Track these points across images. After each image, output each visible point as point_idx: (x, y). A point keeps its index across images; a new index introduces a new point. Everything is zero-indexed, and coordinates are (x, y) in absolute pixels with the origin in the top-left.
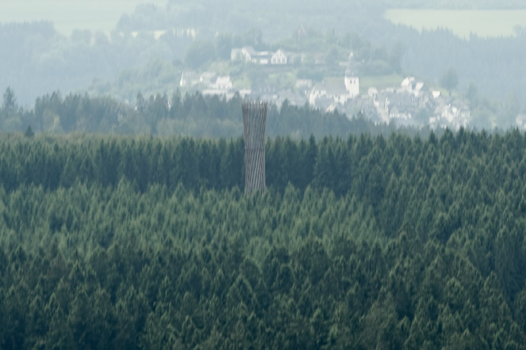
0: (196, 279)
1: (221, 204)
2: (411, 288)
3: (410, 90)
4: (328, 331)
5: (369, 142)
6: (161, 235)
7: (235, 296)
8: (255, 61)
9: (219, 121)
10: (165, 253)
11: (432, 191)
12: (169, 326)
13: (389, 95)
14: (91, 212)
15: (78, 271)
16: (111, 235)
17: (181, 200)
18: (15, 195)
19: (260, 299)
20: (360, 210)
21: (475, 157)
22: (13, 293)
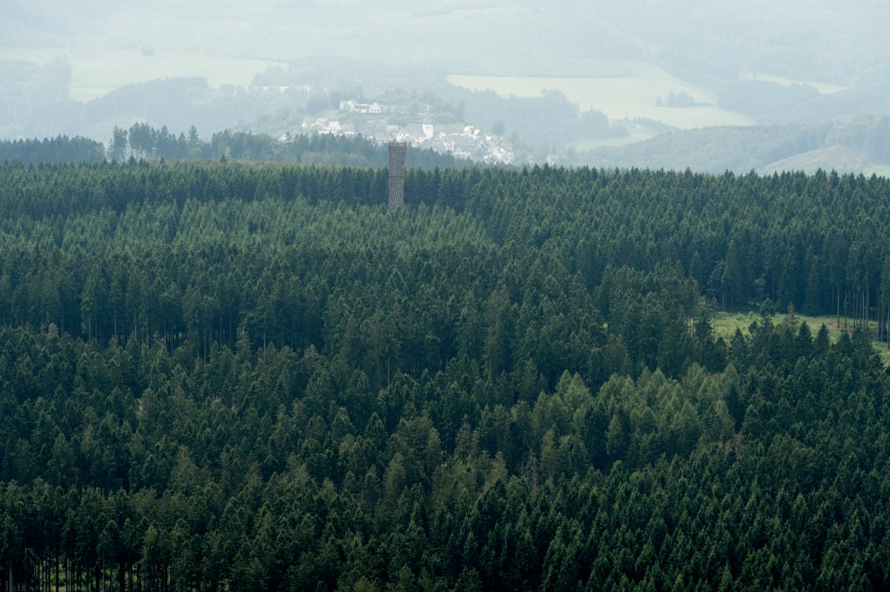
0: (362, 270)
1: (372, 216)
2: (520, 282)
3: (470, 135)
4: (459, 312)
5: (479, 173)
6: (330, 237)
7: (392, 284)
8: (358, 110)
9: (346, 154)
10: (339, 251)
11: (529, 210)
12: (344, 305)
13: (455, 138)
14: (278, 219)
15: (277, 263)
16: (293, 237)
17: (343, 211)
18: (222, 205)
19: (409, 286)
20: (474, 223)
21: (557, 186)
22: (231, 278)
